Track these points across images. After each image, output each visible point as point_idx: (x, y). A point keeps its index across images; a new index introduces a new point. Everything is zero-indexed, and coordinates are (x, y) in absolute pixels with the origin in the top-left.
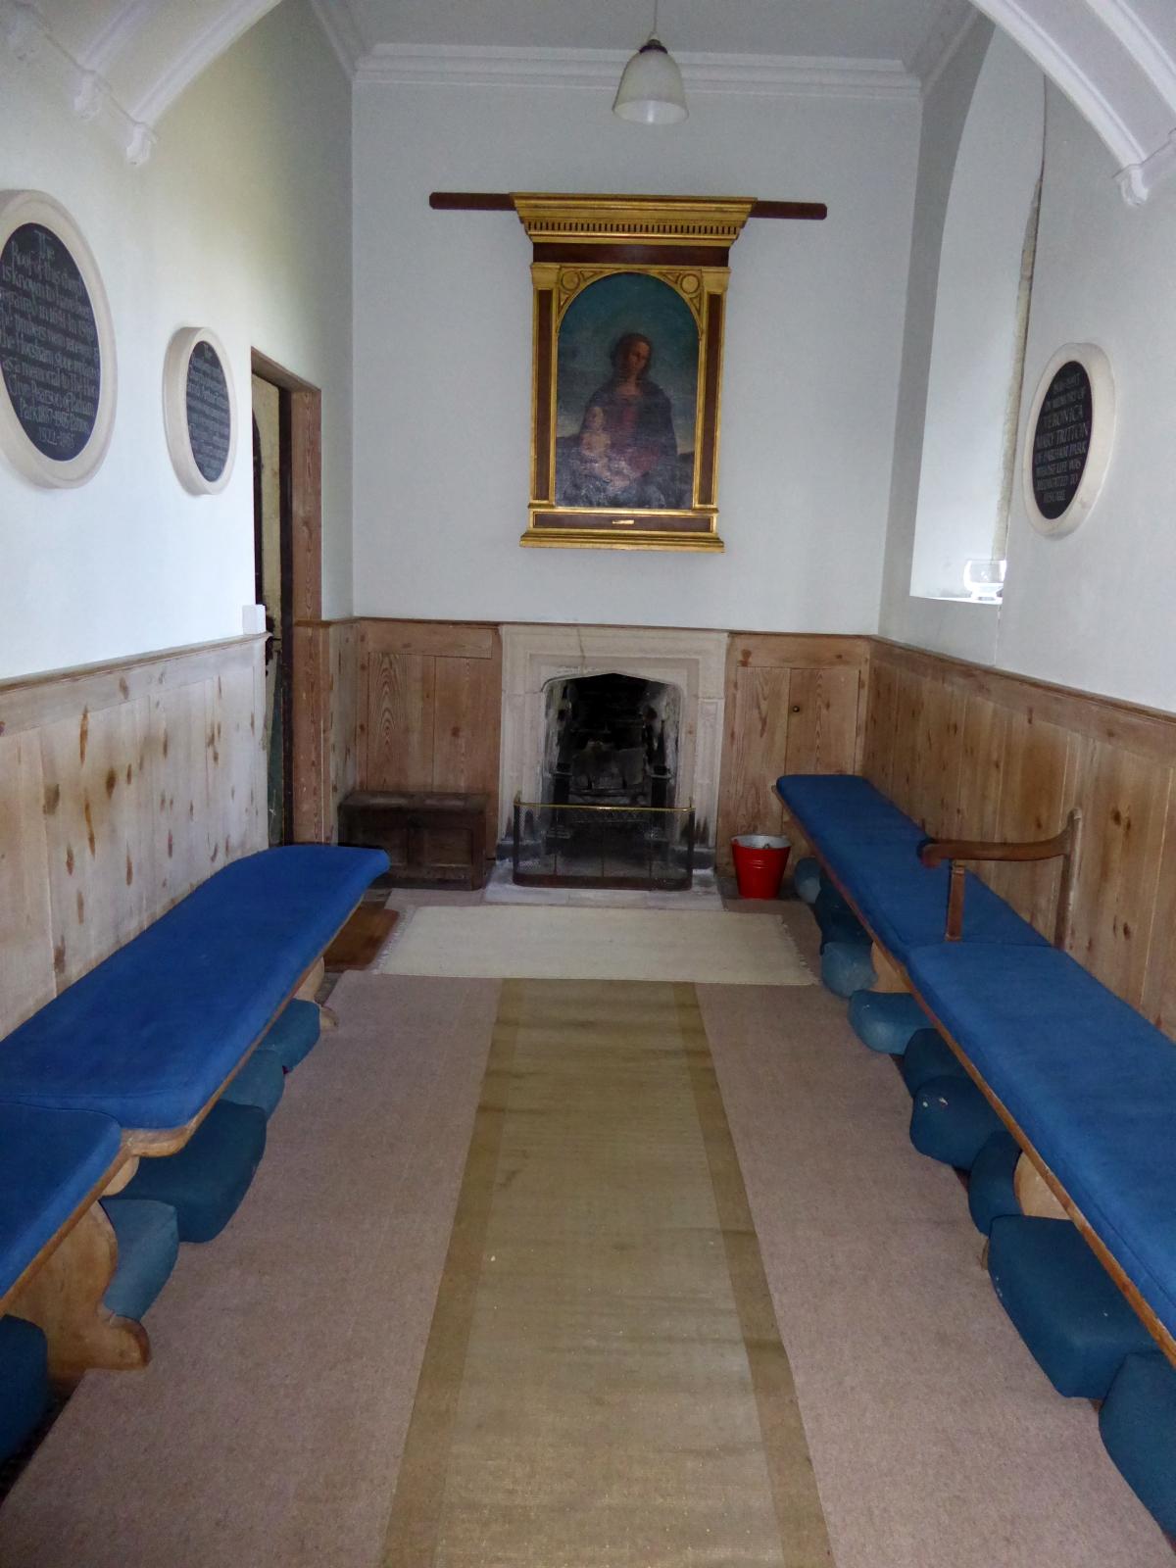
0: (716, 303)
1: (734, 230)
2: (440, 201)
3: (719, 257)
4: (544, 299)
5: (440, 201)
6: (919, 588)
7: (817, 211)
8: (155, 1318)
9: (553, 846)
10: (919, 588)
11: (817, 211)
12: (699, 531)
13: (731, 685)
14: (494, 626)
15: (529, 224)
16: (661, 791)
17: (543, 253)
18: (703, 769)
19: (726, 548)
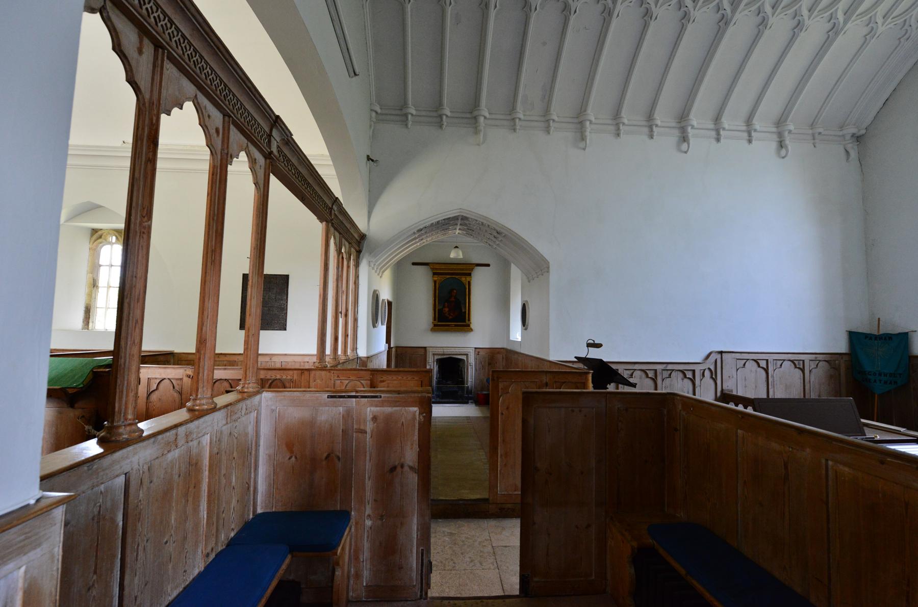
0: (469, 283)
1: (472, 269)
2: (414, 264)
3: (470, 275)
4: (435, 282)
5: (414, 264)
6: (517, 593)
7: (488, 265)
8: (792, 33)
9: (438, 396)
10: (517, 593)
11: (488, 265)
12: (472, 330)
13: (476, 359)
14: (425, 348)
15: (433, 269)
16: (463, 382)
17: (434, 274)
18: (471, 376)
19: (430, 333)
